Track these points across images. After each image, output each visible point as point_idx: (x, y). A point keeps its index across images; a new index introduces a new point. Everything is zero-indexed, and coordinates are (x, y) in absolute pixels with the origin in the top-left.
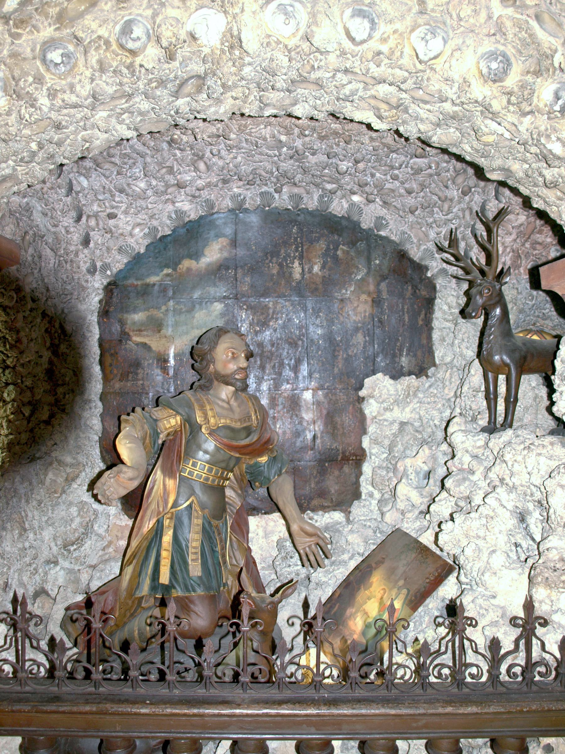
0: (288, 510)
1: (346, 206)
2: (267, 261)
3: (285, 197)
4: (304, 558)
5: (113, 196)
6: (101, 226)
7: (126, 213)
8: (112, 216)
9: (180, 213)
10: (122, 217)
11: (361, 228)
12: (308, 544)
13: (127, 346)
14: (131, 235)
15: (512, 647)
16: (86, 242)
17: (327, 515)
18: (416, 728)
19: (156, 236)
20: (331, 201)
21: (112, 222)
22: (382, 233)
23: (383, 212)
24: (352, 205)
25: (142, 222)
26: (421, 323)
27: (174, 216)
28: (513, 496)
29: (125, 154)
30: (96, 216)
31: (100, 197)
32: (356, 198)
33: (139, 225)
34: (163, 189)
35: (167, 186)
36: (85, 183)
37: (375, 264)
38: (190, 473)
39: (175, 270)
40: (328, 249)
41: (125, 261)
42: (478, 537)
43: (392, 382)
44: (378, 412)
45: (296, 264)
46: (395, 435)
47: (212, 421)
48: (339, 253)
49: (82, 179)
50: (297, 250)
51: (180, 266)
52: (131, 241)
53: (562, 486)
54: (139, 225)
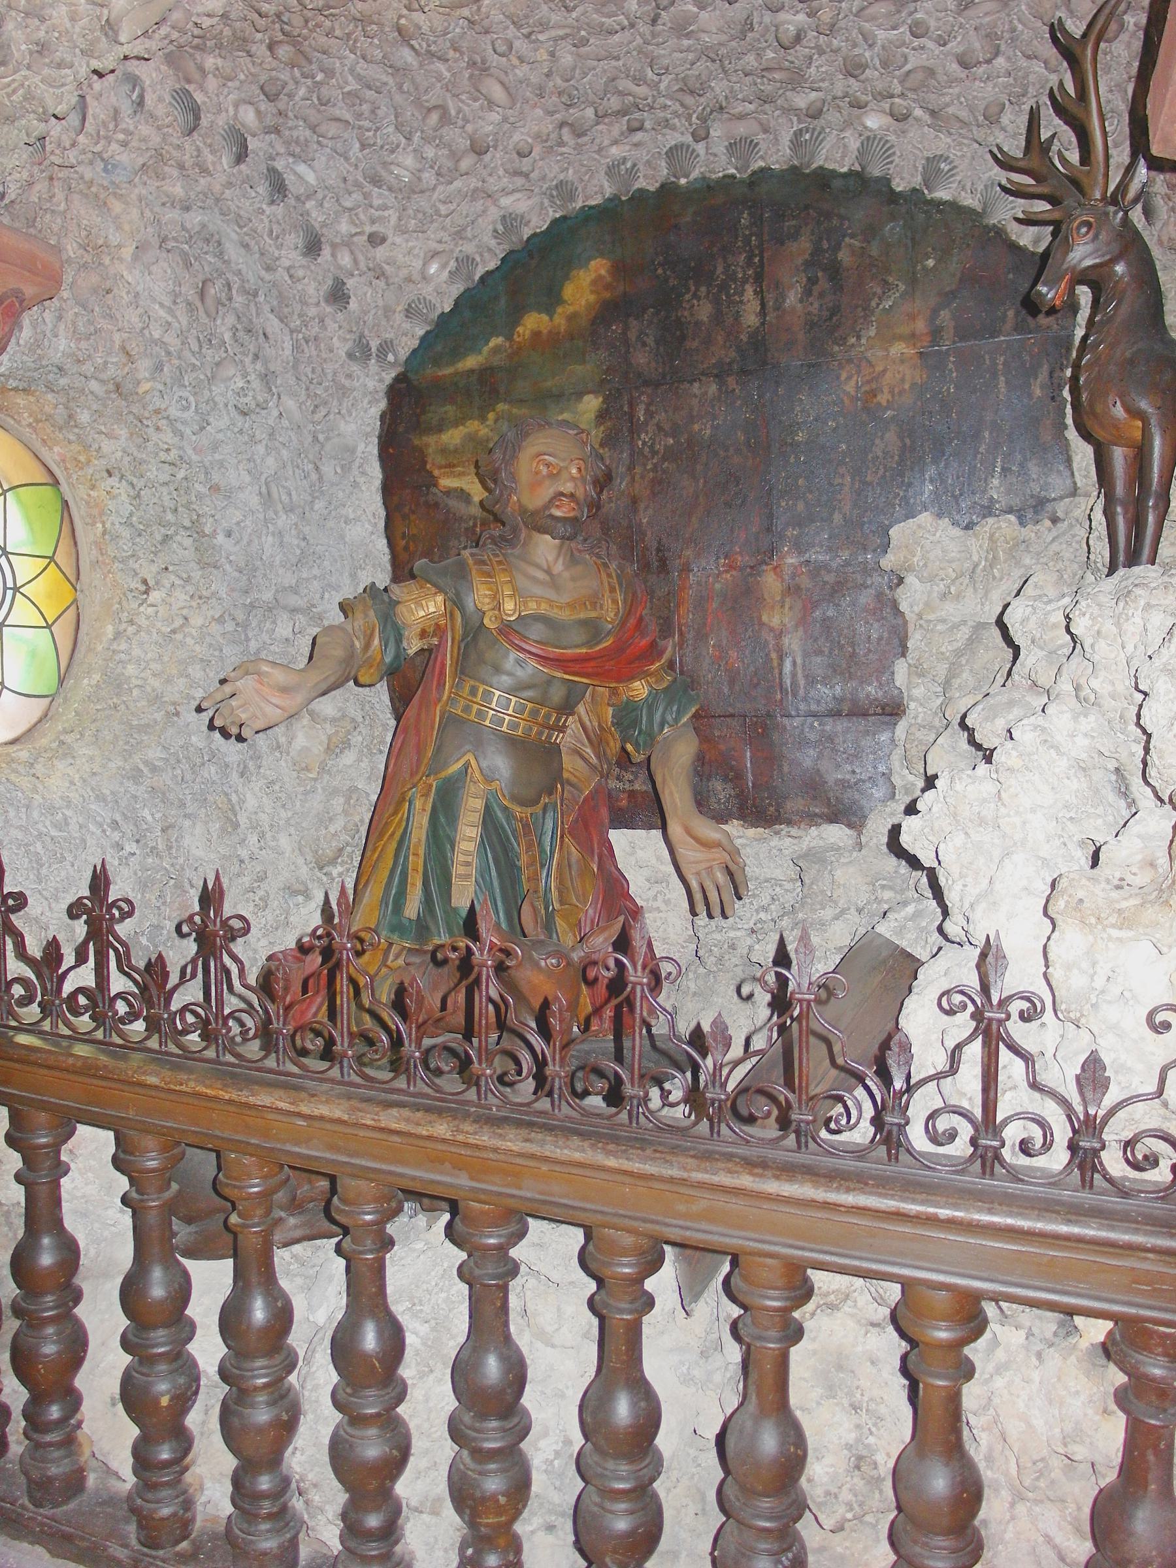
0: (667, 792)
1: (854, 144)
2: (687, 297)
3: (720, 149)
4: (698, 897)
5: (366, 196)
6: (362, 266)
7: (402, 230)
8: (376, 240)
9: (510, 221)
10: (398, 240)
11: (892, 191)
12: (704, 865)
13: (430, 497)
14: (425, 278)
15: (941, 1062)
16: (338, 295)
17: (814, 831)
18: (686, 1216)
19: (470, 277)
20: (818, 137)
21: (381, 252)
22: (942, 194)
23: (941, 143)
24: (869, 141)
25: (440, 248)
26: (1038, 392)
27: (500, 228)
28: (1090, 722)
29: (349, 93)
30: (348, 243)
31: (348, 204)
32: (874, 122)
33: (435, 254)
34: (450, 164)
35: (456, 157)
36: (311, 178)
37: (924, 268)
38: (479, 713)
39: (509, 338)
40: (817, 251)
41: (421, 332)
42: (982, 821)
43: (956, 532)
44: (927, 604)
45: (749, 291)
46: (958, 653)
47: (509, 606)
48: (843, 256)
49: (302, 168)
50: (749, 262)
51: (520, 329)
52: (428, 291)
53: (1167, 671)
54: (435, 254)
